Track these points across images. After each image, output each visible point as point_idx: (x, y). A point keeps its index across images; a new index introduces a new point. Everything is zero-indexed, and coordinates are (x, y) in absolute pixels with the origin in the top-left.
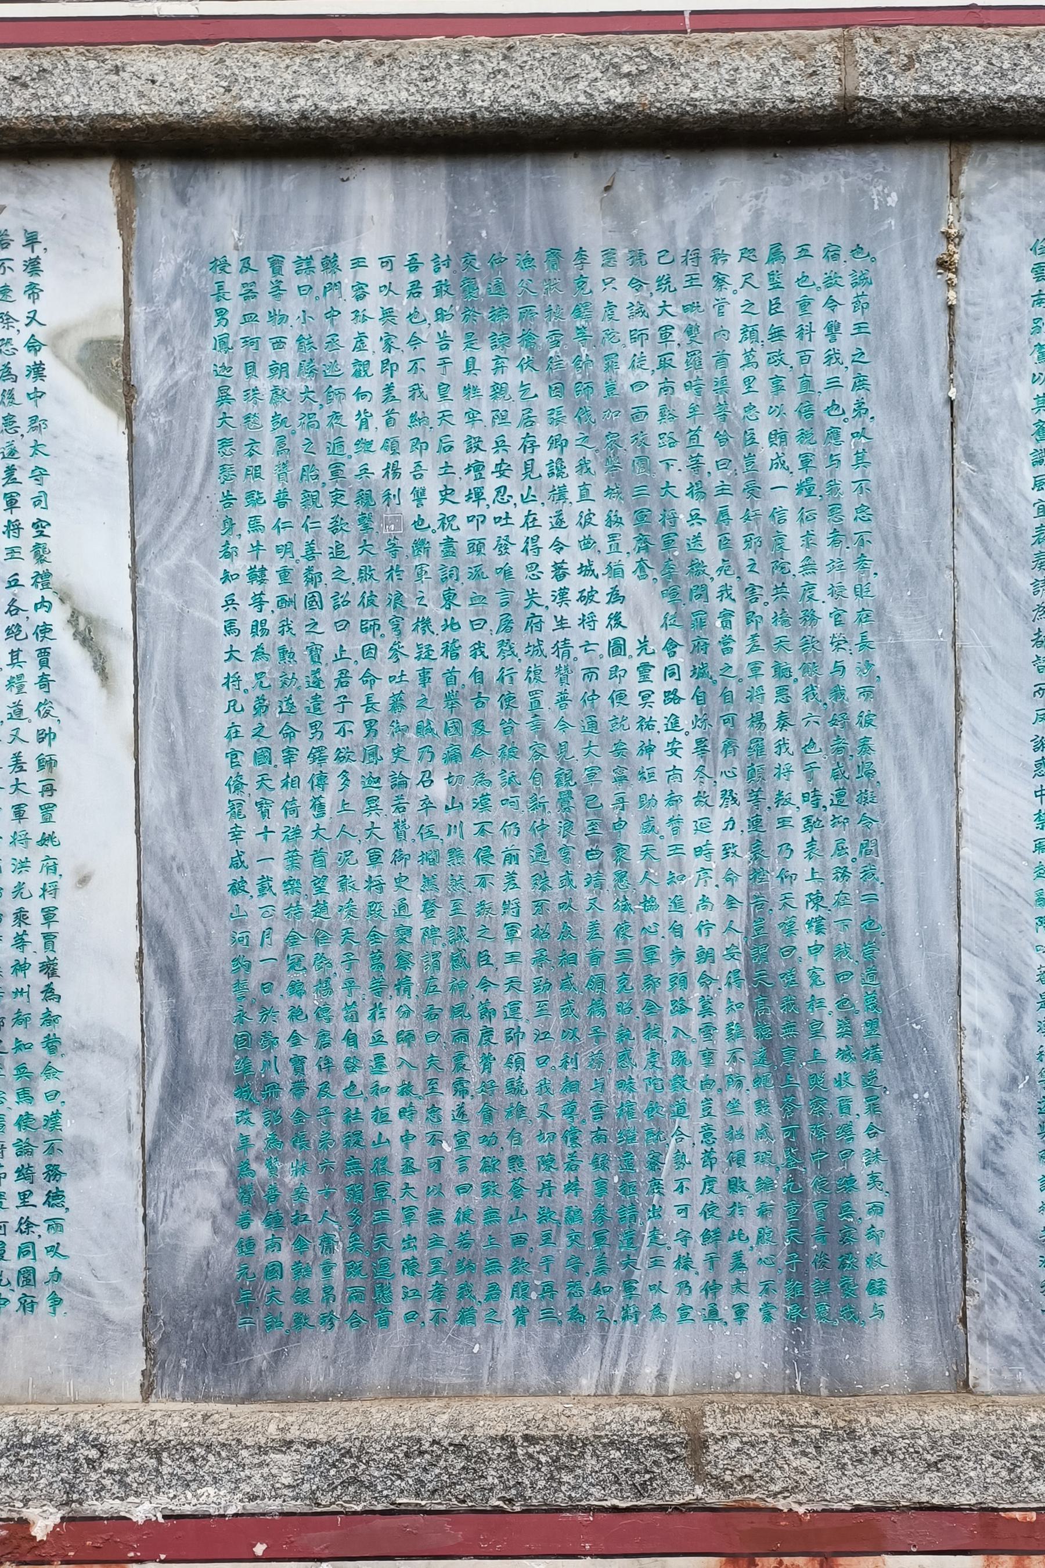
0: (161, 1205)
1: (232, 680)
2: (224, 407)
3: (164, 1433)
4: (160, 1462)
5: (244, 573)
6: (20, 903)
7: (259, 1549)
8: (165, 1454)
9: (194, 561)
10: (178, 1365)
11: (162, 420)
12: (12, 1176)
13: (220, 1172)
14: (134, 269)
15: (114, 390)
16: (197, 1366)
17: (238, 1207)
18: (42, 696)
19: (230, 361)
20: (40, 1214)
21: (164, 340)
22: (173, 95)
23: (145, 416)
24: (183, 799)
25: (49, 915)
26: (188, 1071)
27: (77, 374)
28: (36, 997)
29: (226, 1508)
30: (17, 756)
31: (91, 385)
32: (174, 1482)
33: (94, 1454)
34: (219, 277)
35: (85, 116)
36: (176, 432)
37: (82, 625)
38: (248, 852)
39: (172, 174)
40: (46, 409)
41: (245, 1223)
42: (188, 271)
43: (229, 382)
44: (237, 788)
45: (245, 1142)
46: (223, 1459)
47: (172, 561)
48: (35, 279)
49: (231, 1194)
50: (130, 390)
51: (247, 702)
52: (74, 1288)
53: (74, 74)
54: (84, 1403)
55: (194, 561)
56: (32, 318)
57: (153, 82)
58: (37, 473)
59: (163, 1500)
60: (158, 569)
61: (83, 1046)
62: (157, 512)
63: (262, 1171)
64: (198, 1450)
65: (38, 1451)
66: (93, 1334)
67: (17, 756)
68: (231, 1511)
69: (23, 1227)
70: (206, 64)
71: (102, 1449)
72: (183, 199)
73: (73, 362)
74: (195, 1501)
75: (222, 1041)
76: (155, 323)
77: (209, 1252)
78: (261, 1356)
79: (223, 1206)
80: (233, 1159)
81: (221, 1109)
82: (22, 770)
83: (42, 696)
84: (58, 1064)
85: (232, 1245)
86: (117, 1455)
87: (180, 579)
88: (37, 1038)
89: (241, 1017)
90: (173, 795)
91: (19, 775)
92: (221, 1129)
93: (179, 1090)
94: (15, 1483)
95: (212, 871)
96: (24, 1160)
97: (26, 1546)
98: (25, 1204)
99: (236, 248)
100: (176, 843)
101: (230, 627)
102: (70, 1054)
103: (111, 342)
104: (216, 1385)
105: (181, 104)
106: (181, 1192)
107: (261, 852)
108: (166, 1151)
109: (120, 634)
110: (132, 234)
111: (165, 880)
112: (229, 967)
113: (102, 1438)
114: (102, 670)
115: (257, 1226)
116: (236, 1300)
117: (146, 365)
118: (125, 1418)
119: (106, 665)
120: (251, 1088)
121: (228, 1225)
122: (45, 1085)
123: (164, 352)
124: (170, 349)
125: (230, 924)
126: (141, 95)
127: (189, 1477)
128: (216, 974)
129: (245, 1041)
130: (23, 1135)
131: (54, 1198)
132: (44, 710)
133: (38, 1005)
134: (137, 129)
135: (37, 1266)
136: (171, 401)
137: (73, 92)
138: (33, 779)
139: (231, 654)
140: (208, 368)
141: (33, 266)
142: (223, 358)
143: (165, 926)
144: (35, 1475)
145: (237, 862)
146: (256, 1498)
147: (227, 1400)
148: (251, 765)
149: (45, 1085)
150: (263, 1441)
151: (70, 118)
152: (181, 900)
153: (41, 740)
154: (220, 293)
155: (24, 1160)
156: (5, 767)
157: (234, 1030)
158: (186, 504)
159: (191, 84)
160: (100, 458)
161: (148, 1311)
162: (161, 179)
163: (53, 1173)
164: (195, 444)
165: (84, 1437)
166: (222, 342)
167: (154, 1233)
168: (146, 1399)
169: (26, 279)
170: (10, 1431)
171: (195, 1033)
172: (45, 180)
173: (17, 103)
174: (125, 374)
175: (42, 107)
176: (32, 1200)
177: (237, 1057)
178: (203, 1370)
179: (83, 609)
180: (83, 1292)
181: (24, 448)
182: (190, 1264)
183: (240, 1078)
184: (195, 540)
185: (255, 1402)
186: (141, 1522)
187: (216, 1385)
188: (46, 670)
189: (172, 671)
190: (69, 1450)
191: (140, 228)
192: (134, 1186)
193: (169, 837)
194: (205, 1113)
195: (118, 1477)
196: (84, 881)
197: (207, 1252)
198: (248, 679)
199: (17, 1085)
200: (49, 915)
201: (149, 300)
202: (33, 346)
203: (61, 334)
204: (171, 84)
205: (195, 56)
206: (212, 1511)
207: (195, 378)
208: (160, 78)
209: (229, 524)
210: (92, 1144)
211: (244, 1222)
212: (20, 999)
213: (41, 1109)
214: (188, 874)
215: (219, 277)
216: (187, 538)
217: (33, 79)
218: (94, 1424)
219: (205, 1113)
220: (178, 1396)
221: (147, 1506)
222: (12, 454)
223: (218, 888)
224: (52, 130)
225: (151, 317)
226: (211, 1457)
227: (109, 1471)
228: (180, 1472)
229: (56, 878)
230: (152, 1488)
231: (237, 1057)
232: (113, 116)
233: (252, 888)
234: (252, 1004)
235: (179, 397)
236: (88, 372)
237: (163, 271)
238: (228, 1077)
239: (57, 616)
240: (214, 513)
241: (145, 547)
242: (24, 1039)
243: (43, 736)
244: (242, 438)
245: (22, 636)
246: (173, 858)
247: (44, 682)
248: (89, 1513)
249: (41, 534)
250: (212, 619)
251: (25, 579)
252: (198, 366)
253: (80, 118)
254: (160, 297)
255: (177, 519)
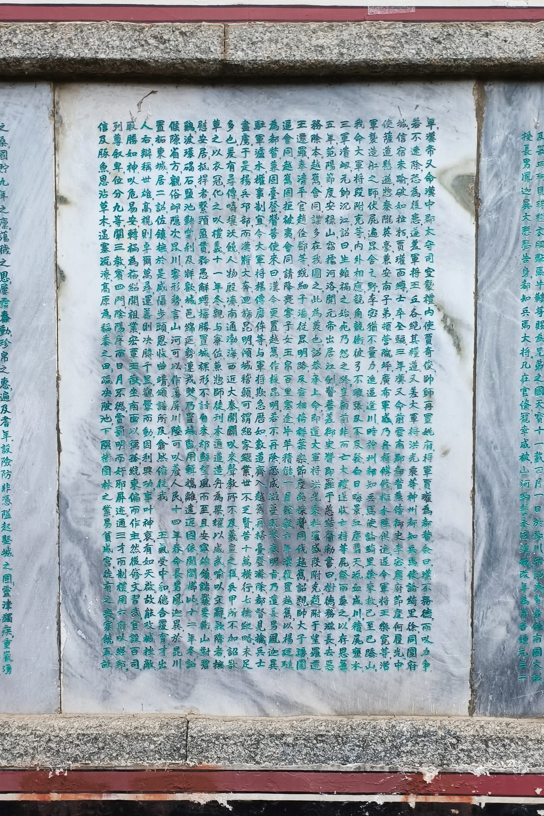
0: (481, 618)
1: (525, 352)
2: (526, 210)
3: (489, 732)
4: (487, 746)
5: (533, 296)
6: (413, 464)
7: (538, 791)
8: (490, 742)
9: (507, 290)
10: (487, 698)
11: (494, 217)
12: (405, 602)
13: (511, 602)
14: (483, 139)
15: (470, 201)
16: (497, 699)
17: (520, 620)
18: (427, 359)
19: (530, 186)
20: (419, 621)
21: (497, 175)
22: (516, 48)
23: (485, 214)
24: (498, 412)
25: (427, 470)
26: (496, 550)
27: (451, 193)
28: (420, 511)
29: (521, 770)
30: (413, 389)
31: (458, 198)
32: (495, 756)
33: (454, 741)
34: (526, 142)
35: (470, 59)
36: (501, 223)
37: (449, 322)
38: (530, 440)
39: (504, 89)
40: (434, 211)
41: (523, 628)
42: (511, 139)
43: (529, 197)
44: (525, 407)
45: (524, 587)
46: (519, 746)
47: (496, 290)
48: (432, 144)
49: (516, 613)
50: (478, 201)
51: (533, 363)
52: (436, 659)
53: (465, 36)
54: (440, 716)
55: (507, 290)
56: (429, 164)
57: (506, 41)
58: (429, 244)
59: (489, 765)
60: (488, 294)
61: (442, 537)
62: (489, 265)
63: (532, 602)
64: (506, 741)
65: (426, 739)
66: (445, 681)
67: (413, 389)
68: (524, 771)
69: (411, 627)
70: (533, 32)
71: (458, 739)
72: (509, 102)
73: (449, 186)
74: (505, 766)
75: (514, 536)
76: (492, 166)
77: (505, 642)
78: (530, 694)
79: (512, 619)
80: (518, 595)
81: (512, 569)
82: (416, 396)
83: (427, 359)
84: (430, 546)
85: (516, 639)
86: (466, 742)
87: (500, 299)
88: (420, 533)
89: (524, 524)
90: (493, 410)
91: (414, 399)
92: (512, 580)
93: (491, 560)
94: (415, 754)
95: (512, 449)
96: (412, 594)
97: (421, 785)
98: (411, 616)
99: (536, 127)
100: (493, 434)
101: (525, 324)
102: (436, 541)
103: (469, 176)
104: (507, 709)
105: (519, 53)
106: (491, 612)
107: (537, 440)
108: (484, 590)
109: (468, 327)
110: (483, 120)
111: (487, 453)
112: (518, 498)
113: (458, 734)
114: (458, 347)
115: (529, 629)
116: (518, 666)
117: (487, 188)
118: (466, 724)
119: (461, 344)
120: (528, 560)
121: (514, 628)
122: (423, 556)
123: (496, 182)
124: (499, 180)
125: (519, 476)
126: (499, 48)
127: (502, 754)
128: (512, 502)
129: (526, 536)
130: (411, 581)
131: (426, 613)
132: (428, 366)
133: (420, 516)
134: (495, 66)
135: (417, 647)
136: (499, 207)
137: (464, 46)
138: (421, 401)
139: (525, 338)
140: (518, 190)
141: (431, 137)
142: (527, 185)
143: (487, 477)
144: (425, 751)
145: (524, 445)
146: (536, 765)
147: (512, 716)
148: (533, 395)
149: (423, 556)
150: (539, 737)
151: (462, 59)
152: (495, 463)
153: (426, 381)
154: (526, 151)
155: (412, 594)
156: (407, 394)
157: (520, 530)
158: (504, 261)
159: (525, 42)
160: (461, 236)
161: (473, 671)
162: (499, 91)
163: (426, 600)
164: (510, 229)
165: (449, 732)
166: (527, 177)
167: (477, 632)
168: (471, 714)
169: (427, 143)
170: (411, 729)
171: (500, 531)
172: (440, 92)
173: (435, 51)
174: (476, 193)
175: (448, 54)
176: (415, 614)
177: (522, 544)
178: (501, 701)
179: (450, 314)
180: (440, 661)
181: (422, 231)
182: (495, 648)
183: (523, 554)
184: (508, 279)
185: (527, 718)
186: (478, 776)
187: (507, 709)
188: (429, 345)
189: (494, 347)
190: (442, 739)
191: (487, 117)
192: (467, 608)
193: (490, 431)
194: (504, 572)
195: (466, 753)
196: (445, 453)
197: (504, 642)
198: (533, 351)
199: (409, 556)
200: (427, 470)
201: (490, 155)
202: (429, 178)
203: (444, 172)
204: (515, 43)
205: (527, 28)
206: (514, 771)
207: (512, 195)
208: (509, 39)
209: (526, 271)
210: (446, 587)
211: (523, 627)
212: (411, 512)
213: (421, 568)
214: (499, 451)
215: (526, 142)
216: (504, 278)
217: (444, 39)
218: (452, 726)
219: (504, 572)
220: (488, 713)
221: (481, 768)
222: (416, 234)
223: (514, 458)
224: (452, 66)
225: (490, 163)
226: (512, 744)
227: (462, 750)
228: (498, 751)
229: (431, 451)
230: (484, 759)
231: (522, 544)
232: (484, 59)
233: (532, 458)
234: (530, 517)
235: (503, 205)
236: (457, 192)
237: (497, 140)
238: (517, 554)
239: (436, 318)
240: (519, 265)
241: (482, 283)
242: (413, 533)
243: (427, 379)
244: (535, 226)
245: (418, 328)
246: (492, 442)
247: (428, 351)
248: (452, 770)
249: (430, 275)
250: (515, 320)
251: (420, 299)
252: (514, 188)
253: (467, 60)
254: (495, 153)
255: (499, 268)
